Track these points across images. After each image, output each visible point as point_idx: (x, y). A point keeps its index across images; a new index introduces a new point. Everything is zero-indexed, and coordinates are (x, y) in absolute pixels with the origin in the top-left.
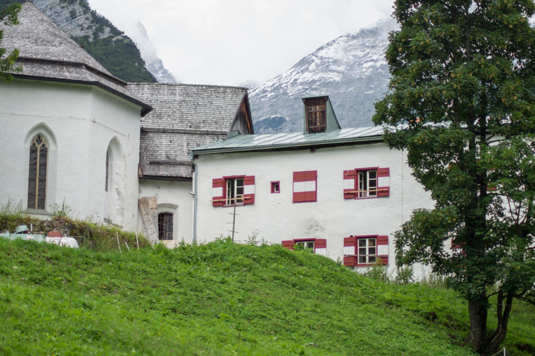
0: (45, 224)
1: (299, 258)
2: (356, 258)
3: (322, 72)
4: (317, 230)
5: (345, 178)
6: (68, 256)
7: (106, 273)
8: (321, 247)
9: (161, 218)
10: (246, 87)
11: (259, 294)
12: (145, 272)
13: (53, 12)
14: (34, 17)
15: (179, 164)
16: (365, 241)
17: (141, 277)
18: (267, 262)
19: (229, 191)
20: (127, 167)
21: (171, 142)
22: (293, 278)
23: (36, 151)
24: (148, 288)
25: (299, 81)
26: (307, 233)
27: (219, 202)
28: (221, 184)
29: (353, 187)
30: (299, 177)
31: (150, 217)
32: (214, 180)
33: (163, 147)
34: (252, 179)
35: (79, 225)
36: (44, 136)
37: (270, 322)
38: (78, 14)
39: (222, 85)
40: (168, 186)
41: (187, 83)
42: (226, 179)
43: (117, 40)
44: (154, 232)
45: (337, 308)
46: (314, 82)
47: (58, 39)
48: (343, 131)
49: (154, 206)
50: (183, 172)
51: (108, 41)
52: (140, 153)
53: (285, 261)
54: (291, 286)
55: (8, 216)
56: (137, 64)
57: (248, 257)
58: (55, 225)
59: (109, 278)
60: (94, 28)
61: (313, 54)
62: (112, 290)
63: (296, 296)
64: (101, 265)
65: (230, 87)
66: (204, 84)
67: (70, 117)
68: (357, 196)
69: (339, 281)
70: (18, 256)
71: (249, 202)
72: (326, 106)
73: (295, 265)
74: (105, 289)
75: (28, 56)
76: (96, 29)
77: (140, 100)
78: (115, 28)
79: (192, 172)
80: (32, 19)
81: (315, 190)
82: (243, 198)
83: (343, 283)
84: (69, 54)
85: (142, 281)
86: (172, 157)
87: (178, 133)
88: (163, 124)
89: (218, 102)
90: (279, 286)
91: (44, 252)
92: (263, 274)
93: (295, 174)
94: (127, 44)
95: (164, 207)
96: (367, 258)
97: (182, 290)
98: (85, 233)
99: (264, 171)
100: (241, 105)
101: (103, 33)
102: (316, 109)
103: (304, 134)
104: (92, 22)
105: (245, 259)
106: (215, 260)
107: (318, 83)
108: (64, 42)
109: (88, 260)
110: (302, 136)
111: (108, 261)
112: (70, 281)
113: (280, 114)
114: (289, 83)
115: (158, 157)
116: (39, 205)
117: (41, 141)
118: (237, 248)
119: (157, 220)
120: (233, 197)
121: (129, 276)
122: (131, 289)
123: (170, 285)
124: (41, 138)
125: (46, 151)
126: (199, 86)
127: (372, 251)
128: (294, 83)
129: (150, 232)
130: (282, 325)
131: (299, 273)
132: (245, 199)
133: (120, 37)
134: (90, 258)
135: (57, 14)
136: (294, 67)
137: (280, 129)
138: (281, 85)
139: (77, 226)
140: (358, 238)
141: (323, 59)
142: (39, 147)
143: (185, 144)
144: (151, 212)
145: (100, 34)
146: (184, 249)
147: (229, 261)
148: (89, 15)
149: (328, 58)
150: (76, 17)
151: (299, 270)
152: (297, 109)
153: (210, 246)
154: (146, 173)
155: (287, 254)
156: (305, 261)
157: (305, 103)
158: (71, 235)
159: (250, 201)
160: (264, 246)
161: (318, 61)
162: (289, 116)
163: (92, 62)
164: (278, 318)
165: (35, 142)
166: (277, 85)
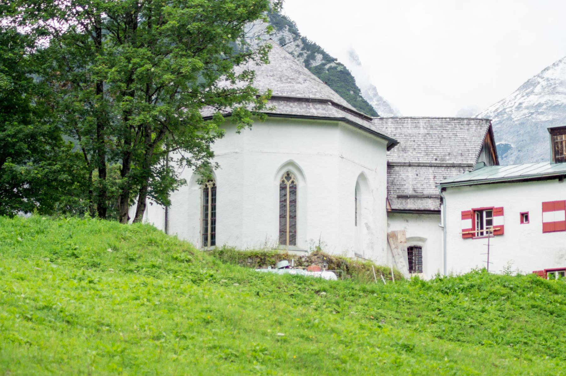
0: (303, 260)
3: (549, 94)
6: (335, 288)
7: (372, 304)
11: (518, 321)
14: (277, 55)
15: (426, 197)
17: (406, 308)
18: (524, 291)
19: (478, 223)
20: (375, 201)
21: (417, 175)
22: (550, 306)
23: (286, 188)
24: (413, 317)
25: (524, 105)
27: (469, 234)
29: (470, 227)
31: (399, 250)
32: (462, 212)
33: (410, 180)
36: (293, 173)
37: (532, 347)
38: (287, 41)
41: (430, 116)
42: (474, 211)
43: (330, 68)
44: (404, 266)
46: (540, 105)
49: (403, 240)
50: (431, 205)
51: (320, 69)
53: (540, 290)
55: (267, 253)
56: (352, 92)
57: (504, 286)
58: (313, 260)
59: (375, 308)
60: (305, 55)
61: (538, 76)
63: (555, 323)
64: (366, 296)
66: (448, 117)
70: (289, 289)
71: (498, 233)
73: (550, 293)
76: (308, 57)
77: (385, 135)
78: (327, 55)
79: (440, 204)
84: (314, 90)
85: (406, 311)
86: (419, 190)
87: (423, 166)
88: (409, 157)
89: (463, 133)
90: (538, 314)
91: (312, 285)
92: (521, 303)
94: (341, 71)
97: (446, 319)
98: (342, 267)
99: (512, 201)
100: (486, 137)
101: (315, 60)
102: (562, 139)
103: (551, 164)
104: (303, 49)
105: (502, 288)
106: (472, 290)
107: (545, 107)
108: (308, 79)
109: (354, 292)
110: (549, 166)
111: (373, 292)
112: (338, 312)
113: (505, 141)
114: (514, 108)
115: (406, 191)
116: (290, 241)
117: (290, 178)
118: (493, 279)
119: (407, 254)
120: (482, 228)
121: (395, 306)
122: (397, 319)
123: (433, 314)
124: (290, 175)
125: (296, 188)
128: (519, 107)
130: (543, 350)
131: (556, 301)
132: (495, 231)
133: (333, 65)
134: (356, 290)
136: (518, 90)
137: (506, 157)
138: (504, 109)
139: (334, 260)
141: (549, 81)
142: (288, 184)
143: (431, 177)
144: (400, 246)
145: (311, 61)
146: (441, 280)
147: (486, 291)
149: (555, 79)
150: (285, 45)
152: (523, 135)
153: (467, 277)
154: (394, 207)
155: (542, 283)
156: (560, 290)
157: (551, 133)
158: (329, 269)
159: (499, 232)
160: (519, 276)
161: (544, 83)
162: (514, 143)
163: (337, 98)
164: (539, 344)
165: (284, 179)
166: (500, 110)
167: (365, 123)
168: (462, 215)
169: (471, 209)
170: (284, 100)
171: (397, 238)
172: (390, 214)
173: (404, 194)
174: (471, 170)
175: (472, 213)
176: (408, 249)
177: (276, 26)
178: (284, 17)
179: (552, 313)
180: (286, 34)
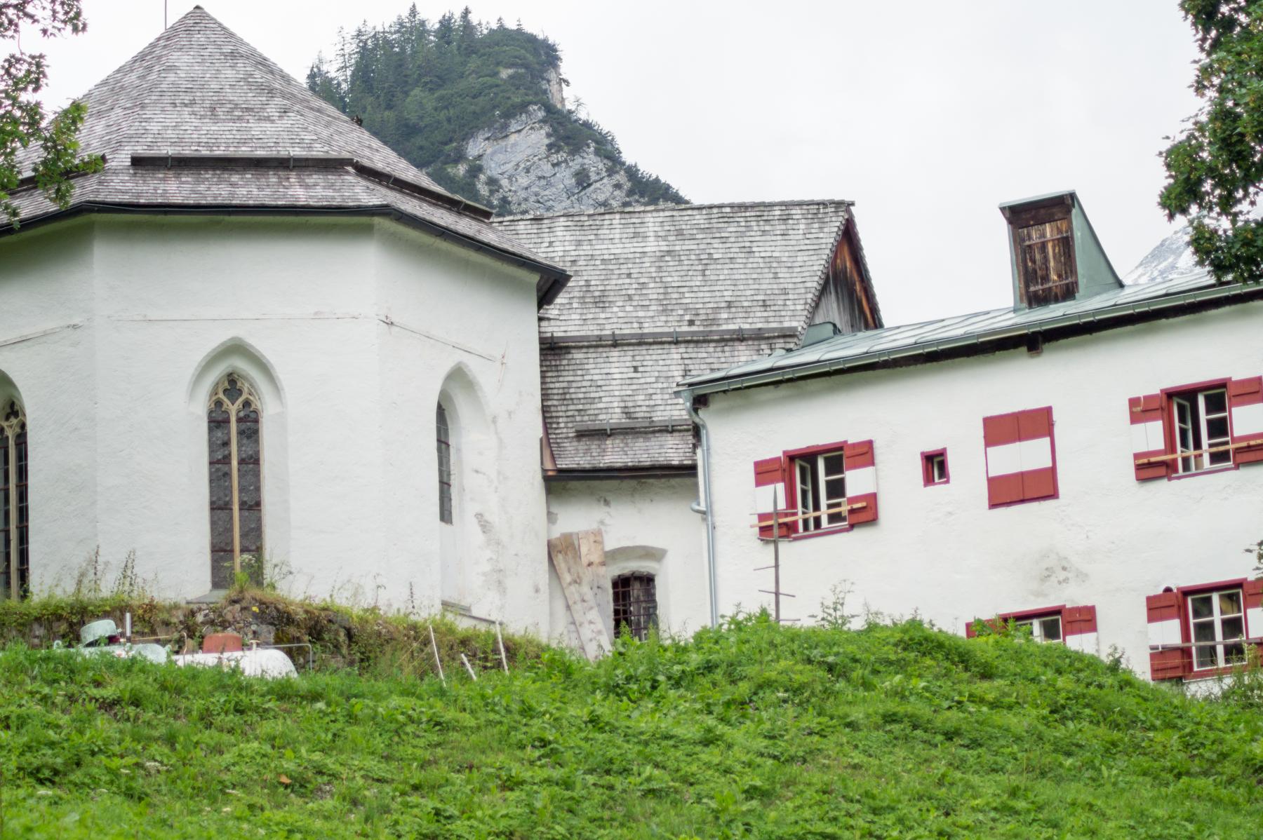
0: (200, 618)
1: (979, 654)
2: (1186, 652)
4: (1066, 580)
5: (1135, 418)
6: (179, 691)
8: (1081, 632)
9: (620, 589)
10: (847, 199)
12: (437, 724)
13: (532, 176)
14: (211, 49)
15: (660, 431)
16: (1208, 601)
19: (804, 493)
20: (505, 447)
21: (636, 369)
26: (1038, 594)
28: (779, 474)
29: (1159, 444)
30: (1001, 430)
31: (585, 589)
32: (757, 464)
33: (611, 385)
34: (865, 449)
35: (307, 612)
36: (245, 378)
38: (593, 177)
42: (792, 457)
44: (599, 632)
45: (1085, 796)
48: (1127, 291)
50: (671, 450)
52: (545, 410)
54: (939, 738)
55: (90, 604)
57: (809, 661)
58: (229, 617)
62: (310, 786)
65: (800, 204)
66: (726, 202)
67: (318, 316)
68: (1176, 471)
69: (1105, 716)
71: (862, 517)
72: (1070, 223)
73: (966, 675)
74: (286, 786)
75: (188, 152)
79: (695, 446)
81: (1049, 464)
82: (844, 509)
83: (1120, 720)
88: (615, 321)
89: (770, 246)
91: (98, 684)
93: (989, 423)
95: (628, 559)
96: (1220, 650)
97: (557, 773)
100: (836, 252)
102: (1043, 235)
104: (630, 193)
115: (601, 417)
117: (240, 392)
118: (778, 640)
120: (817, 507)
124: (239, 384)
125: (256, 421)
126: (711, 207)
127: (1234, 627)
129: (586, 632)
132: (852, 511)
135: (543, 182)
136: (1141, 264)
140: (1186, 593)
142: (233, 409)
144: (587, 575)
148: (621, 177)
150: (589, 185)
151: (978, 692)
154: (564, 464)
156: (1001, 664)
159: (865, 514)
160: (872, 627)
163: (384, 158)
165: (221, 395)
167: (465, 225)
168: (757, 474)
169: (780, 454)
170: (214, 168)
171: (577, 554)
172: (554, 484)
173: (597, 425)
174: (792, 346)
176: (615, 585)
177: (567, 144)
178: (587, 125)
179: (949, 736)
180: (590, 160)
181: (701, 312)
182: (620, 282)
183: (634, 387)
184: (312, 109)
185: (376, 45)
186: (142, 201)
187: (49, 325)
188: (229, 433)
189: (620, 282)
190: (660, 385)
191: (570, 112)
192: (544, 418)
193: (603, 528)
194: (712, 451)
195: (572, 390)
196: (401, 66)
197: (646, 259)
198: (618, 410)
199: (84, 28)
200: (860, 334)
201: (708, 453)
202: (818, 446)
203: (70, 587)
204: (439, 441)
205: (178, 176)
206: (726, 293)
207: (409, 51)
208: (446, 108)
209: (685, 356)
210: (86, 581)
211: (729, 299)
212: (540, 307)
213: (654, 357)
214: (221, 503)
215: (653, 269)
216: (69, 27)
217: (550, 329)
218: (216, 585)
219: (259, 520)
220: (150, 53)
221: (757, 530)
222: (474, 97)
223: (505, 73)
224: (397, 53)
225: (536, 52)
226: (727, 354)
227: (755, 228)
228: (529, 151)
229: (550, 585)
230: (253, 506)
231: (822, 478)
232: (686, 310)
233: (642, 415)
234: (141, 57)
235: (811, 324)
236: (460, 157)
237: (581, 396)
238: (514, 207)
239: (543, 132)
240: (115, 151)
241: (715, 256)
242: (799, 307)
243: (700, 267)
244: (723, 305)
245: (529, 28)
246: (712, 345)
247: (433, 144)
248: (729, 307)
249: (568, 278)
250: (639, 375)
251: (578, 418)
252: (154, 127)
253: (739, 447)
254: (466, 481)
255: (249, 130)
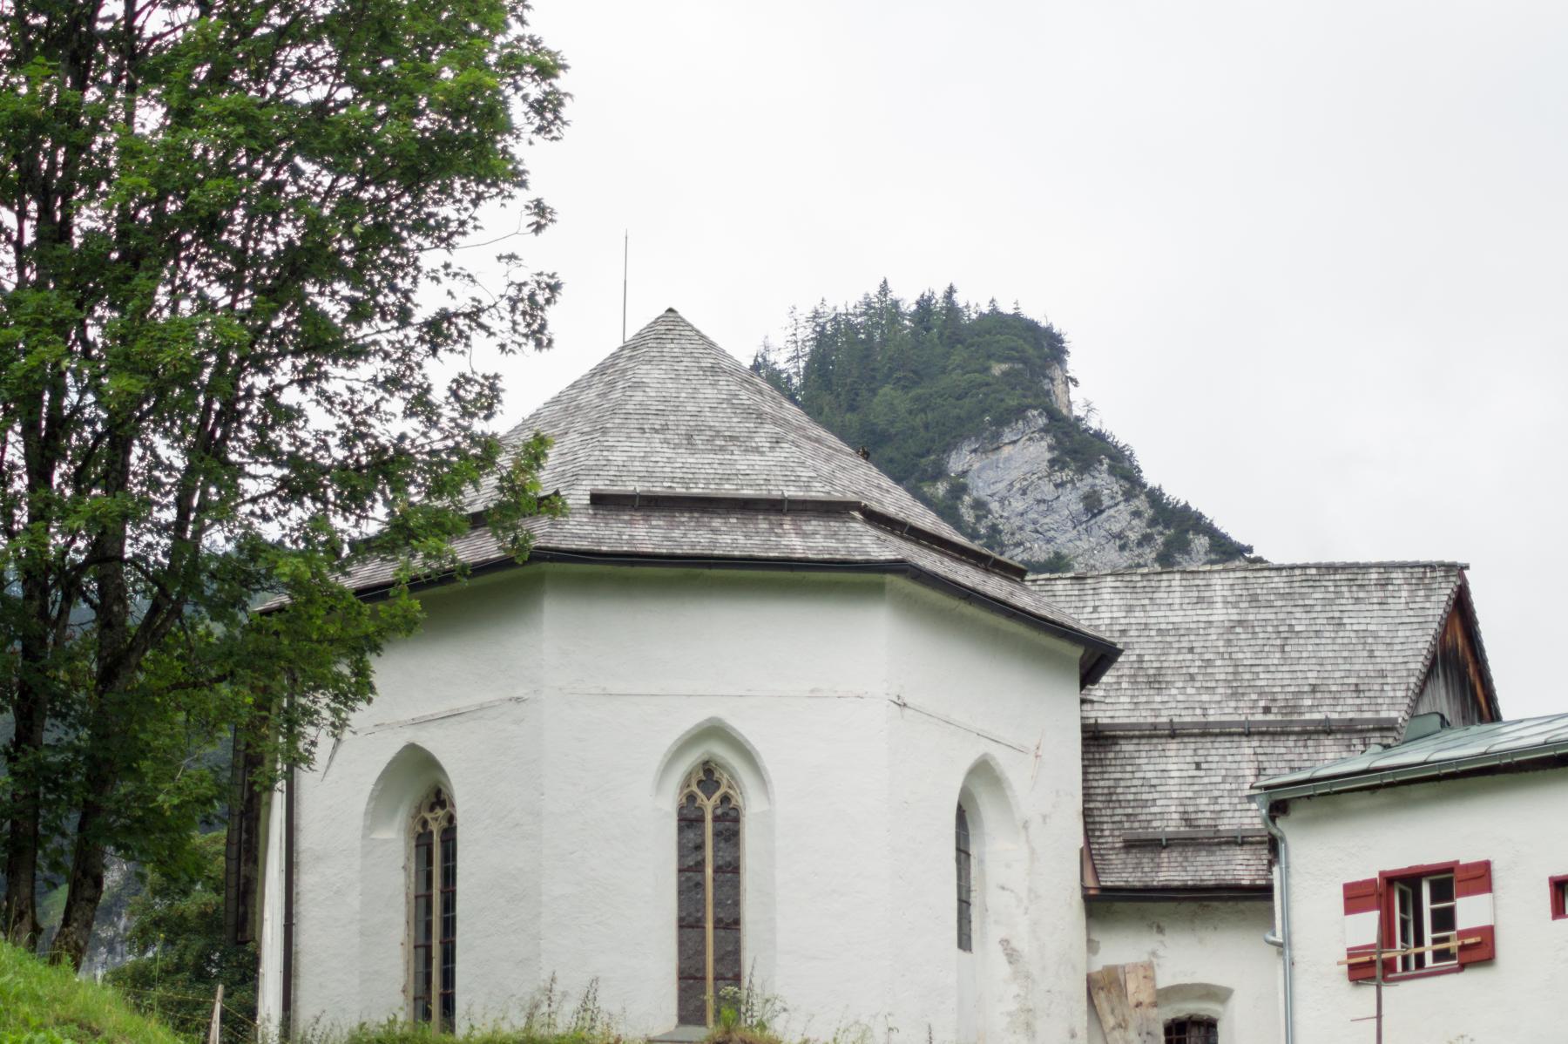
9: (1174, 1037)
10: (1461, 561)
13: (1030, 499)
14: (687, 362)
15: (1227, 843)
19: (1404, 924)
21: (1198, 766)
23: (701, 820)
32: (1348, 888)
33: (1170, 786)
34: (1481, 872)
36: (723, 767)
38: (1106, 502)
39: (1374, 560)
40: (1192, 921)
42: (1390, 879)
47: (769, 428)
49: (1145, 997)
50: (1241, 867)
52: (1087, 813)
60: (1160, 540)
65: (1402, 566)
66: (1312, 561)
67: (814, 694)
71: (1475, 955)
75: (659, 489)
76: (1166, 544)
78: (1224, 537)
80: (680, 367)
82: (1453, 945)
86: (1204, 820)
88: (1173, 705)
89: (1363, 617)
95: (1185, 999)
100: (1446, 626)
101: (1188, 553)
104: (1152, 523)
108: (791, 436)
115: (1155, 824)
117: (718, 784)
120: (1419, 941)
124: (717, 775)
125: (737, 820)
126: (1292, 568)
132: (1463, 948)
135: (1043, 507)
142: (709, 805)
144: (1135, 1017)
150: (1101, 512)
154: (1109, 880)
159: (1479, 951)
163: (895, 500)
165: (694, 788)
167: (995, 586)
168: (1347, 899)
173: (1150, 834)
174: (1390, 741)
175: (1382, 890)
177: (1074, 459)
178: (1099, 436)
180: (1103, 481)
181: (1279, 697)
182: (1180, 657)
183: (1196, 788)
184: (809, 438)
185: (837, 330)
186: (604, 548)
187: (487, 697)
188: (703, 834)
189: (1180, 657)
190: (1228, 786)
191: (1078, 419)
192: (1086, 823)
193: (1155, 961)
194: (1292, 870)
195: (1119, 790)
196: (867, 357)
197: (1212, 631)
198: (1175, 816)
199: (550, 341)
200: (1475, 729)
201: (1287, 872)
202: (1422, 867)
203: (521, 1023)
204: (959, 850)
205: (646, 519)
206: (1309, 675)
207: (877, 338)
208: (923, 410)
209: (1259, 750)
210: (538, 1013)
211: (1312, 681)
212: (1082, 687)
213: (1221, 752)
214: (691, 919)
215: (1221, 643)
216: (532, 343)
217: (1093, 714)
218: (684, 1019)
219: (737, 942)
220: (613, 365)
221: (1345, 967)
222: (958, 399)
223: (998, 369)
224: (863, 341)
225: (1037, 345)
226: (1311, 750)
227: (1347, 595)
228: (1026, 468)
229: (1088, 1028)
230: (730, 924)
231: (1427, 906)
232: (1260, 694)
233: (1205, 822)
234: (601, 370)
235: (1413, 715)
236: (939, 473)
237: (1131, 797)
238: (1005, 538)
239: (1044, 444)
240: (570, 486)
241: (1297, 628)
242: (1399, 694)
243: (1278, 642)
244: (1306, 689)
245: (1031, 312)
246: (1293, 738)
247: (906, 456)
248: (1313, 691)
249: (1119, 652)
250: (1202, 773)
251: (1127, 825)
252: (618, 458)
253: (1325, 867)
254: (990, 899)
255: (733, 463)
